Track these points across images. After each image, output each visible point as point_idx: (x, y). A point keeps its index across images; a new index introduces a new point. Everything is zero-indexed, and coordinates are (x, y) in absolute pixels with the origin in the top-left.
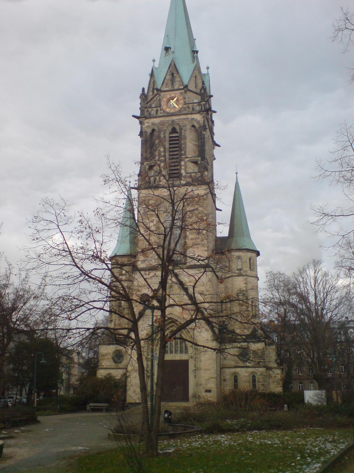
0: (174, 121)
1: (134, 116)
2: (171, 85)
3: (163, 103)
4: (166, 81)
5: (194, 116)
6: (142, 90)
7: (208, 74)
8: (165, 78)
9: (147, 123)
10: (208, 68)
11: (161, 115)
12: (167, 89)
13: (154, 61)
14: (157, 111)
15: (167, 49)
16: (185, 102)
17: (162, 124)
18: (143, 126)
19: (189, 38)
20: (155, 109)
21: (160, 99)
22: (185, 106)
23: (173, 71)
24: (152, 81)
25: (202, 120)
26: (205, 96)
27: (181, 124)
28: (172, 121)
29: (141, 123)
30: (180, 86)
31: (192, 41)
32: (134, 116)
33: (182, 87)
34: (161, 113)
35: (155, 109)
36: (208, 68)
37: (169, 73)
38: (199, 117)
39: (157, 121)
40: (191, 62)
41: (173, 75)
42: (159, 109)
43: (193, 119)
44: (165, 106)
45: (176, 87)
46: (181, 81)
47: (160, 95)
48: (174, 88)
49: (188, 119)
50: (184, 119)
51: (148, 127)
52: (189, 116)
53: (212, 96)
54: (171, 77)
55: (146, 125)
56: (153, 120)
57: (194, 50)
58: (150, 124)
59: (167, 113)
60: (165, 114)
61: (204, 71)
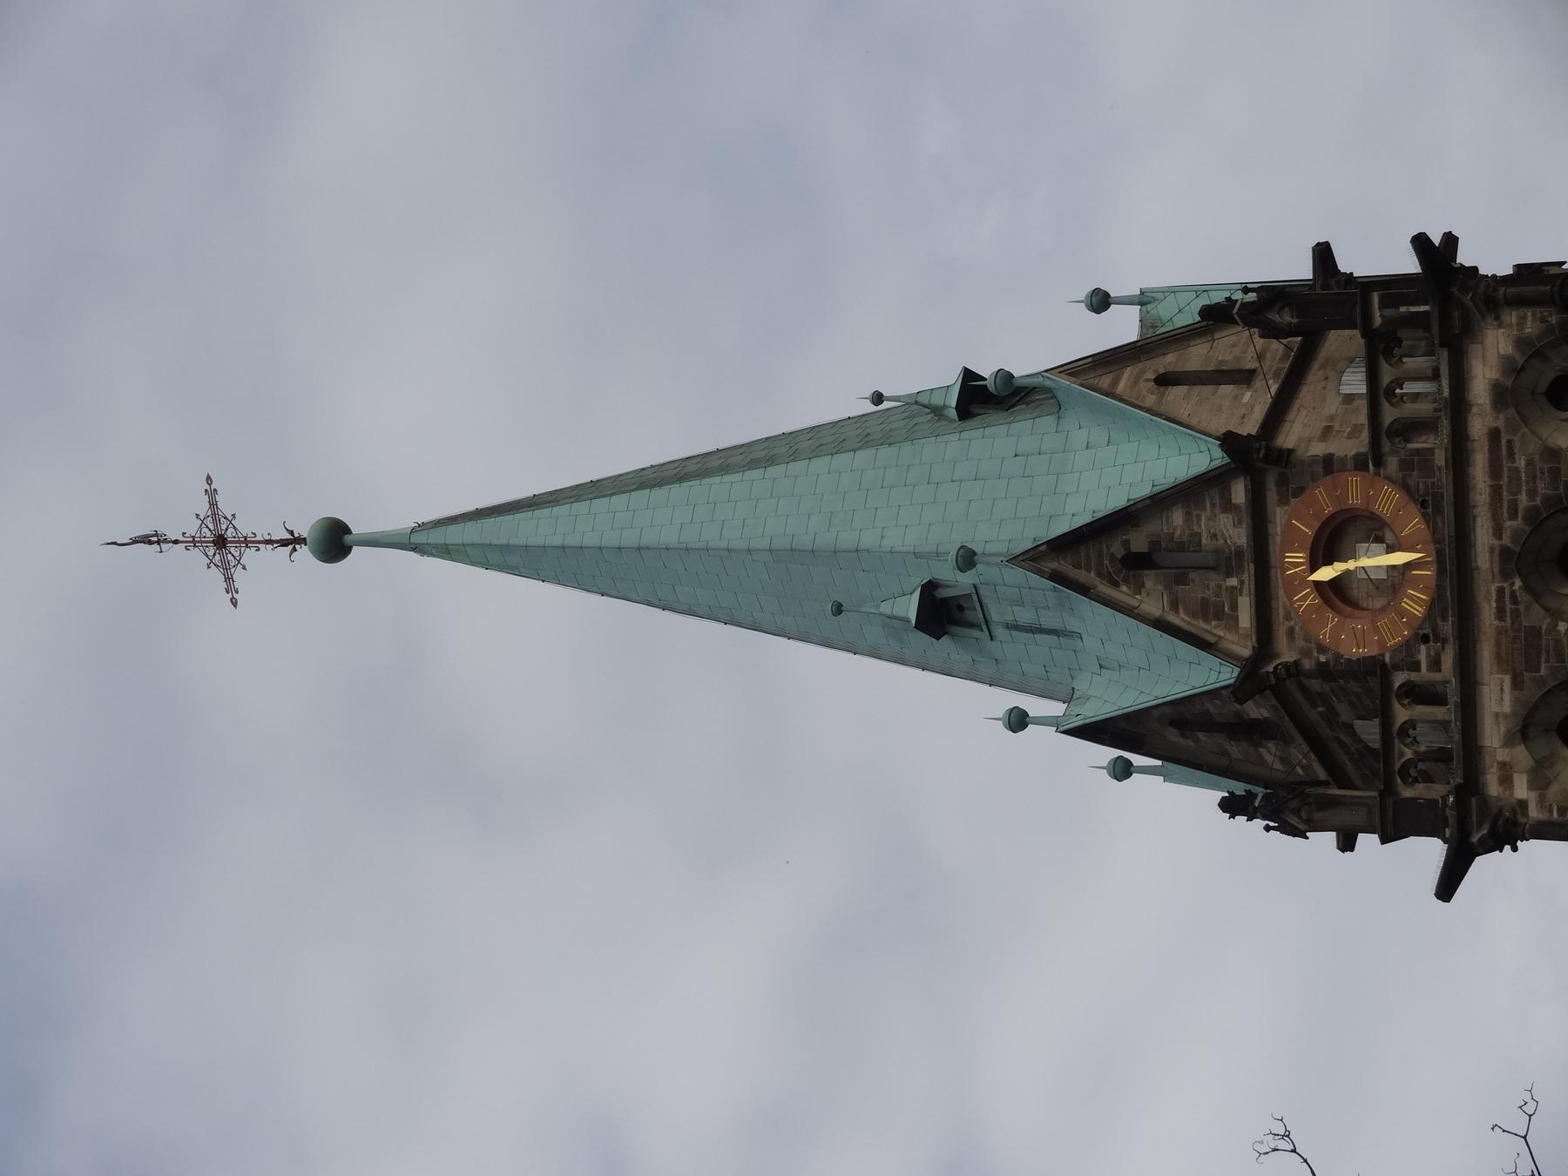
0: (1505, 553)
1: (1447, 888)
2: (1214, 579)
3: (1353, 639)
4: (1179, 619)
5: (1483, 376)
6: (1241, 819)
7: (1143, 299)
8: (1160, 625)
9: (1506, 781)
10: (1100, 302)
11: (1448, 659)
12: (1246, 618)
13: (1018, 721)
14: (1418, 694)
15: (942, 615)
16: (1360, 464)
17: (1524, 652)
18: (1534, 813)
19: (866, 442)
20: (1402, 714)
21: (1324, 671)
22: (1392, 464)
23: (1103, 555)
24: (1173, 735)
25: (1512, 317)
26: (1313, 309)
27: (1532, 494)
28: (1505, 575)
29: (1507, 831)
30: (1228, 506)
31: (890, 424)
32: (1447, 888)
33: (1239, 492)
34: (1436, 664)
35: (1402, 714)
36: (1100, 302)
37: (1123, 594)
38: (1492, 352)
39: (1497, 699)
40: (1047, 422)
41: (1137, 564)
42: (1399, 679)
43: (1501, 396)
44: (1382, 622)
45: (1239, 536)
46: (1188, 493)
47: (1293, 670)
48: (1239, 553)
49: (1494, 435)
50: (1495, 470)
51: (1540, 778)
52: (1478, 426)
53: (1323, 255)
54: (1150, 580)
55: (1521, 790)
56: (1492, 735)
57: (953, 401)
58: (1521, 756)
59: (1436, 608)
60: (1447, 627)
61: (1122, 327)
